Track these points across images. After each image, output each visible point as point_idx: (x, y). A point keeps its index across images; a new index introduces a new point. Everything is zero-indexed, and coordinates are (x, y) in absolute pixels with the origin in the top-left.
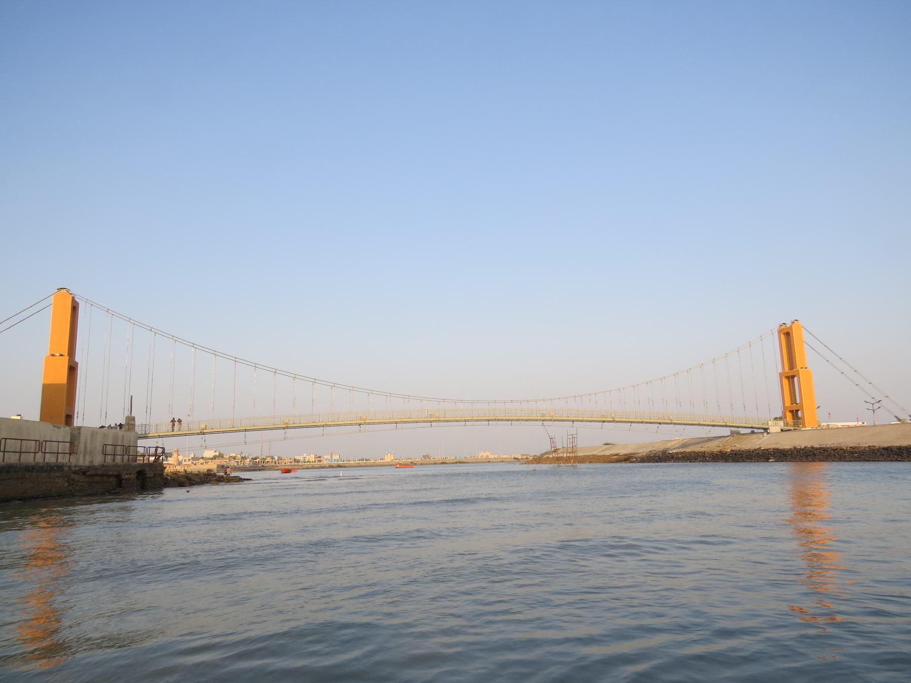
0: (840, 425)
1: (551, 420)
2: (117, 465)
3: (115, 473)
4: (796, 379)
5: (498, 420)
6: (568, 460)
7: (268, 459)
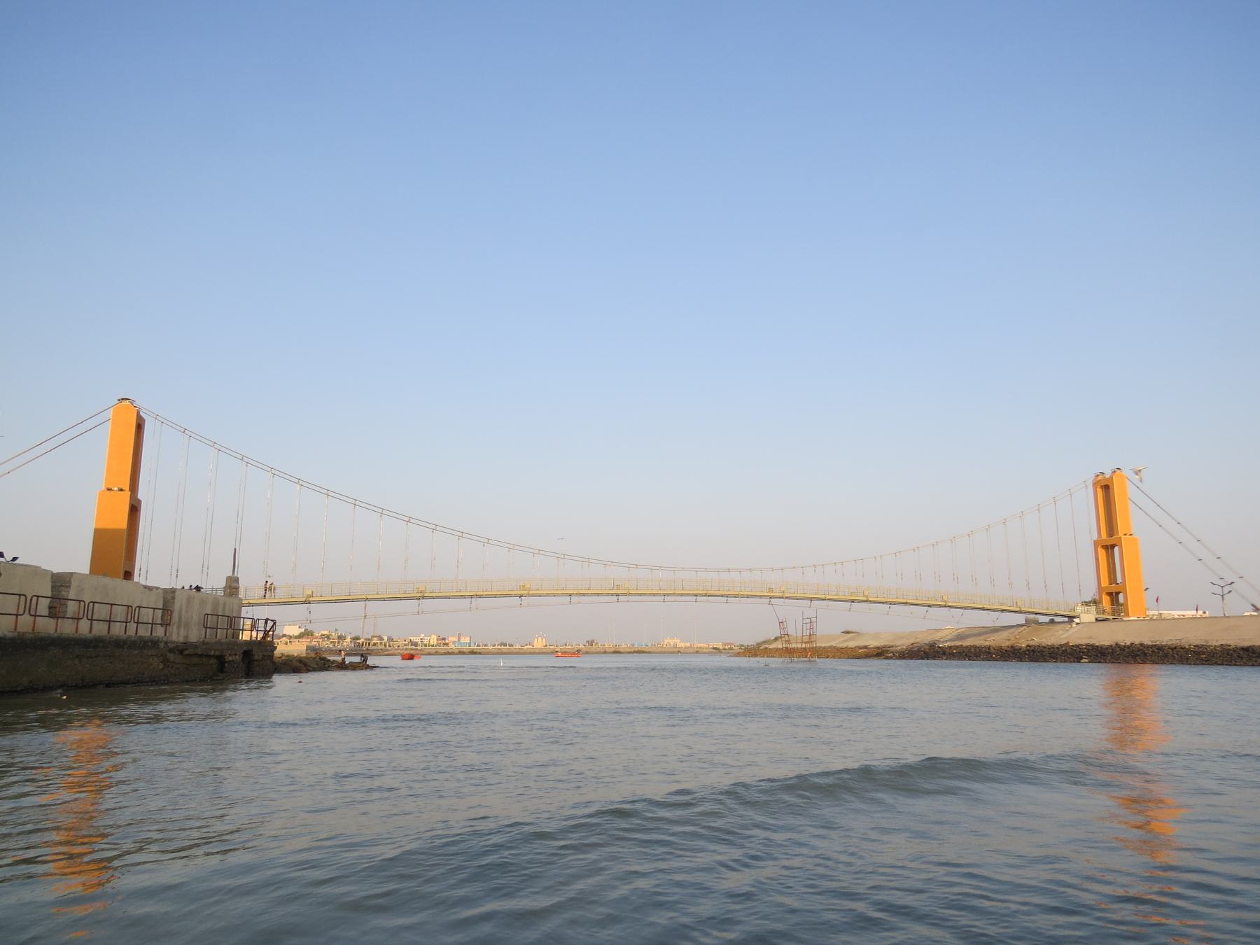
0: (1176, 614)
1: (781, 597)
2: (219, 643)
3: (217, 653)
4: (1116, 549)
5: (710, 595)
6: (803, 652)
7: (375, 640)
